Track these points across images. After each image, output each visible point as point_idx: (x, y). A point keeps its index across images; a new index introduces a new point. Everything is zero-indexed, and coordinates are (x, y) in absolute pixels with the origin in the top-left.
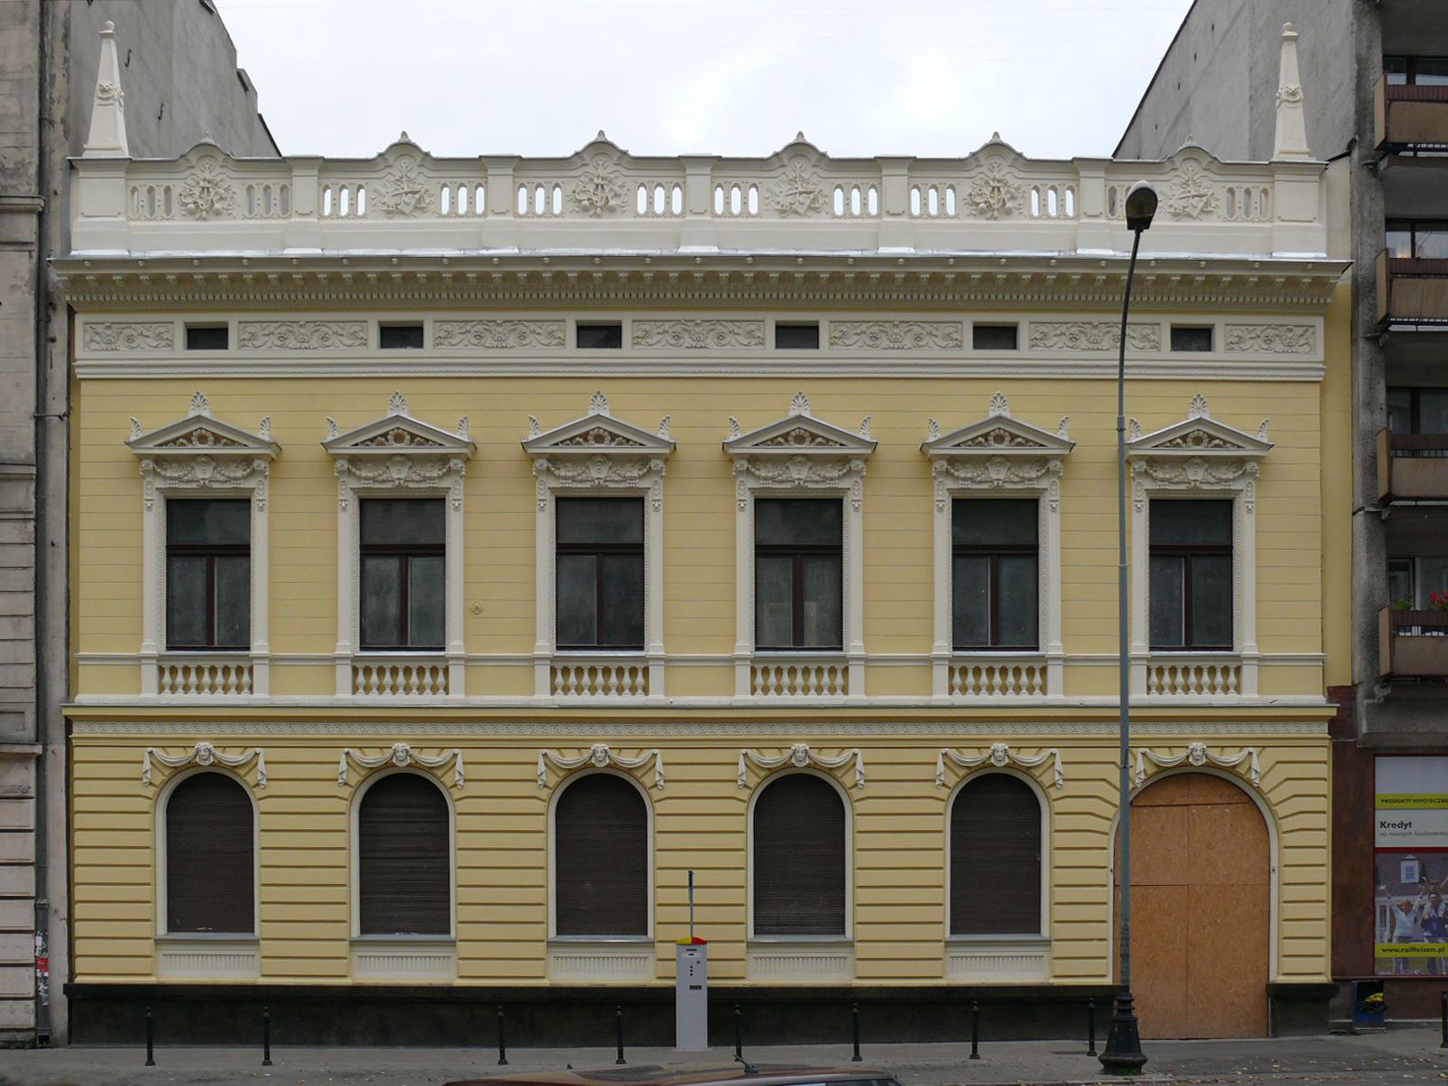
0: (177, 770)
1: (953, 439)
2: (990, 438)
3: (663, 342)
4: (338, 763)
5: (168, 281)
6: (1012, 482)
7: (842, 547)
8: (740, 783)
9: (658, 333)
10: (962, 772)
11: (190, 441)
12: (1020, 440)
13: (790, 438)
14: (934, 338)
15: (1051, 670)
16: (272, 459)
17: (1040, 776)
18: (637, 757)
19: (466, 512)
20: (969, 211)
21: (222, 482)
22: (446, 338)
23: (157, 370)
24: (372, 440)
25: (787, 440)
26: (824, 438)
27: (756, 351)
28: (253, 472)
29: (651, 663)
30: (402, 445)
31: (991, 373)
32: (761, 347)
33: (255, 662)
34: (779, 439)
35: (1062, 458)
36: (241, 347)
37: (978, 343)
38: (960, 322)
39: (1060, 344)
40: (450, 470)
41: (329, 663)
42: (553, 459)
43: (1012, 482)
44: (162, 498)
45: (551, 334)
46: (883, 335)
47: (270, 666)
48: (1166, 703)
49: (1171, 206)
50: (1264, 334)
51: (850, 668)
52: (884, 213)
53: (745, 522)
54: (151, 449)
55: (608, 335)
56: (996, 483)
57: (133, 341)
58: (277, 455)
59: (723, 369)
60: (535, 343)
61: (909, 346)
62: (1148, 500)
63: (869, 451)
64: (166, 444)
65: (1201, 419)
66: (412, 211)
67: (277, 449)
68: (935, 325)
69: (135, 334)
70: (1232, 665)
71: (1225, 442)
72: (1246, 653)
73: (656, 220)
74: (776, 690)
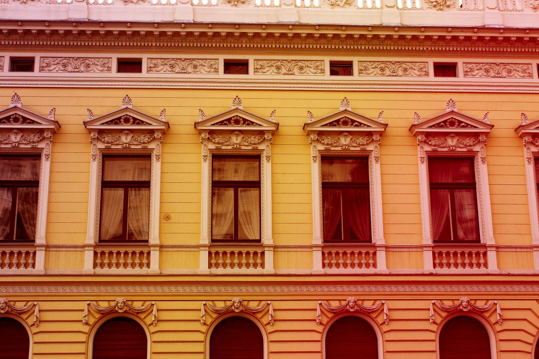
0: (103, 313)
1: (535, 124)
2: (122, 120)
3: (271, 71)
4: (316, 310)
5: (3, 33)
6: (460, 147)
7: (475, 184)
8: (202, 322)
9: (477, 69)
10: (444, 314)
11: (338, 124)
12: (463, 124)
13: (340, 123)
14: (517, 72)
15: (489, 253)
16: (56, 131)
17: (376, 317)
18: (142, 306)
19: (162, 163)
20: (428, 6)
21: (25, 144)
22: (46, 67)
23: (508, 88)
24: (217, 123)
25: (338, 124)
26: (358, 122)
27: (319, 77)
28: (44, 138)
29: (37, 249)
30: (454, 128)
31: (133, 85)
32: (323, 74)
33: (152, 248)
34: (442, 124)
35: (486, 134)
36: (40, 71)
37: (436, 74)
38: (427, 63)
39: (57, 69)
40: (373, 140)
41: (419, 250)
42: (211, 132)
43: (460, 147)
44: (101, 154)
45: (524, 71)
46: (387, 68)
47: (497, 252)
48: (475, 273)
49: (531, 4)
50: (169, 63)
51: (377, 252)
52: (384, 7)
53: (423, 169)
54: (98, 126)
55: (241, 67)
56: (451, 148)
57: (89, 67)
58: (58, 130)
59: (279, 85)
60: (202, 71)
61: (401, 74)
62: (211, 155)
63: (274, 129)
64: (326, 125)
65: (16, 107)
66: (344, 5)
67: (58, 127)
68: (517, 65)
69: (408, 68)
70: (259, 251)
71: (361, 124)
72: (489, 243)
73: (315, 9)
74: (336, 265)
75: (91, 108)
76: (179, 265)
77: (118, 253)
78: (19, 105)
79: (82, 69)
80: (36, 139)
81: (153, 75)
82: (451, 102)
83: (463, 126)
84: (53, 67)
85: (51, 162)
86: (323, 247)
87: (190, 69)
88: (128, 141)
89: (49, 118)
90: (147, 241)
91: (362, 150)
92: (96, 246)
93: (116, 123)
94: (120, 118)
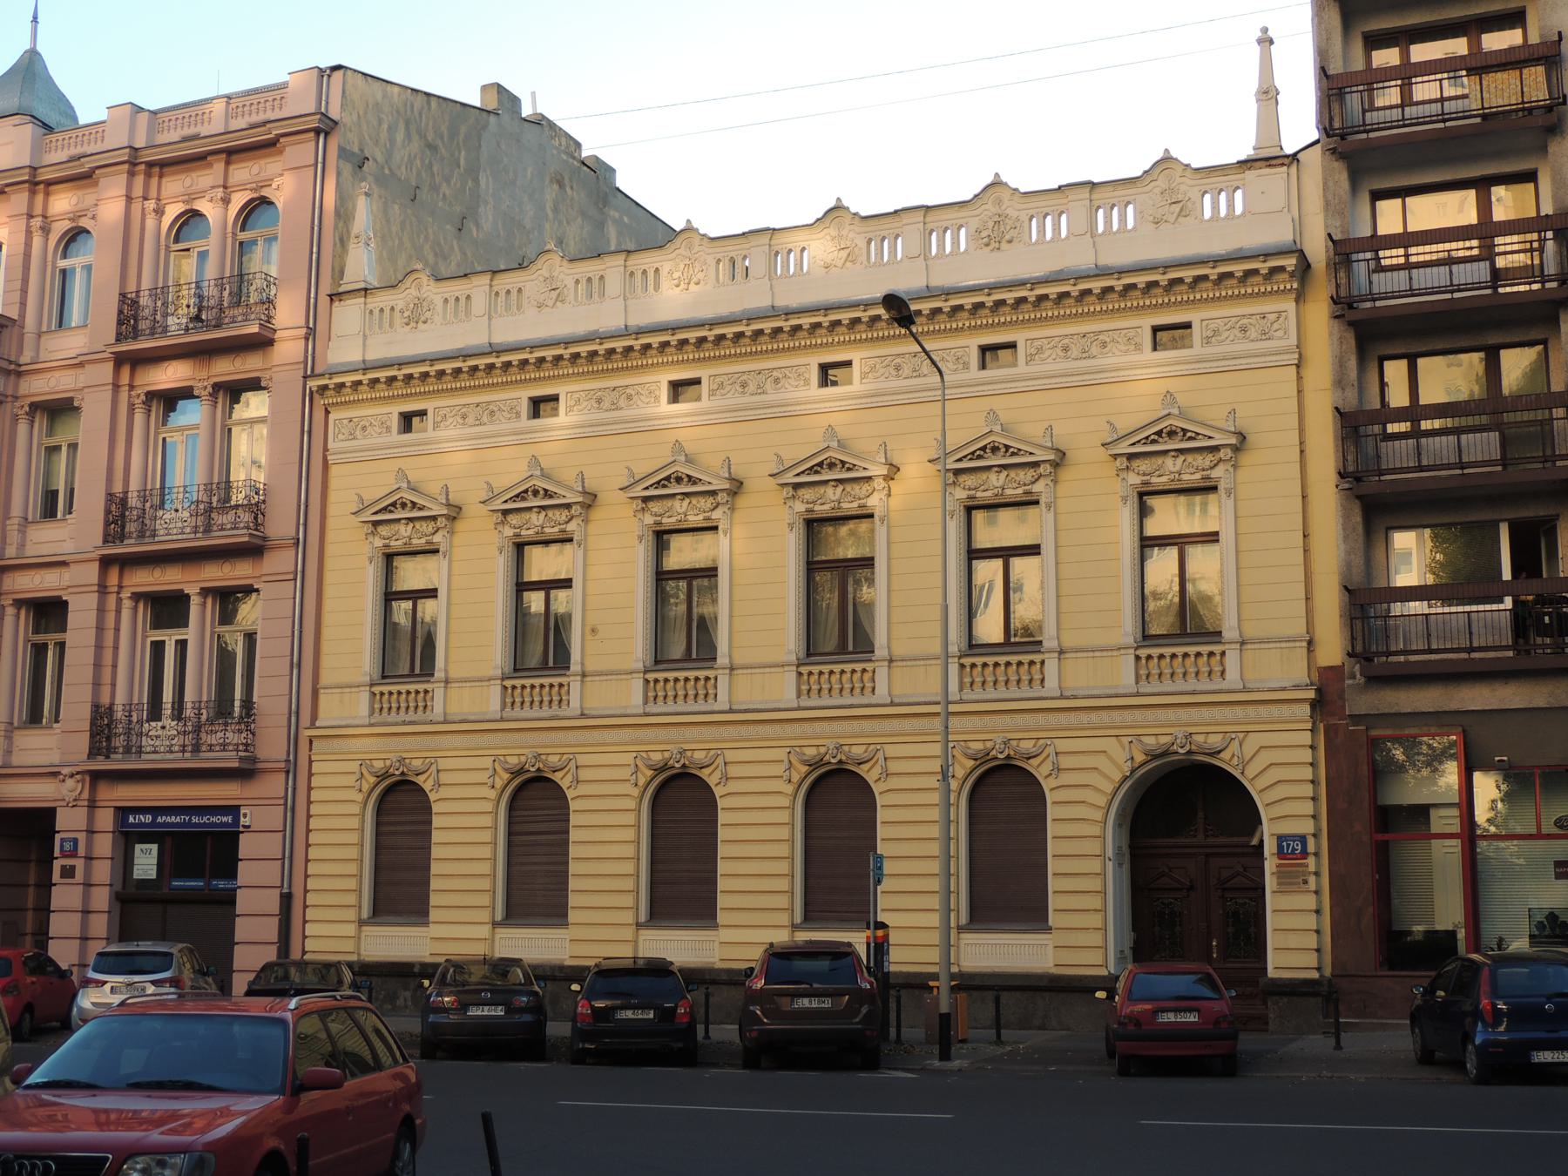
75: (1112, 419)
76: (1082, 676)
77: (523, 687)
78: (1176, 411)
79: (485, 419)
80: (1207, 464)
81: (1035, 368)
82: (992, 414)
83: (1191, 438)
84: (1048, 353)
85: (585, 550)
86: (502, 679)
87: (1094, 350)
88: (1177, 468)
89: (1042, 442)
90: (1040, 642)
91: (1026, 493)
92: (372, 685)
93: (524, 499)
94: (526, 491)
